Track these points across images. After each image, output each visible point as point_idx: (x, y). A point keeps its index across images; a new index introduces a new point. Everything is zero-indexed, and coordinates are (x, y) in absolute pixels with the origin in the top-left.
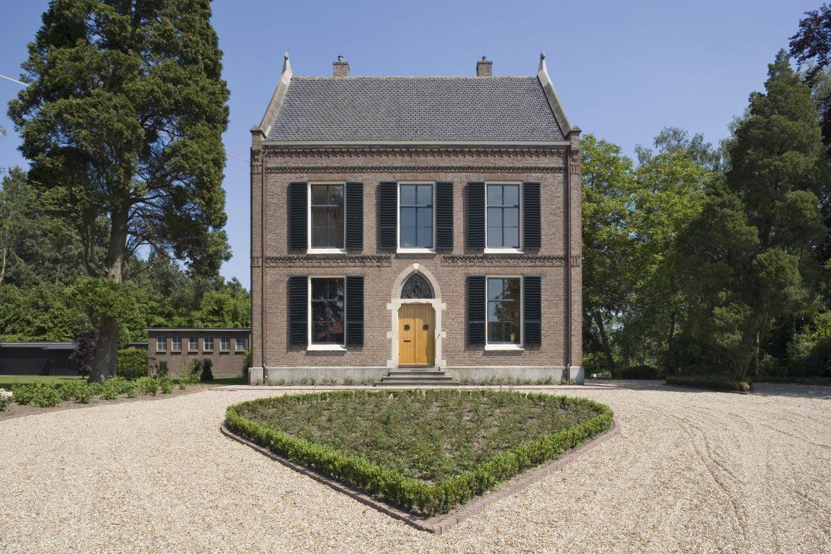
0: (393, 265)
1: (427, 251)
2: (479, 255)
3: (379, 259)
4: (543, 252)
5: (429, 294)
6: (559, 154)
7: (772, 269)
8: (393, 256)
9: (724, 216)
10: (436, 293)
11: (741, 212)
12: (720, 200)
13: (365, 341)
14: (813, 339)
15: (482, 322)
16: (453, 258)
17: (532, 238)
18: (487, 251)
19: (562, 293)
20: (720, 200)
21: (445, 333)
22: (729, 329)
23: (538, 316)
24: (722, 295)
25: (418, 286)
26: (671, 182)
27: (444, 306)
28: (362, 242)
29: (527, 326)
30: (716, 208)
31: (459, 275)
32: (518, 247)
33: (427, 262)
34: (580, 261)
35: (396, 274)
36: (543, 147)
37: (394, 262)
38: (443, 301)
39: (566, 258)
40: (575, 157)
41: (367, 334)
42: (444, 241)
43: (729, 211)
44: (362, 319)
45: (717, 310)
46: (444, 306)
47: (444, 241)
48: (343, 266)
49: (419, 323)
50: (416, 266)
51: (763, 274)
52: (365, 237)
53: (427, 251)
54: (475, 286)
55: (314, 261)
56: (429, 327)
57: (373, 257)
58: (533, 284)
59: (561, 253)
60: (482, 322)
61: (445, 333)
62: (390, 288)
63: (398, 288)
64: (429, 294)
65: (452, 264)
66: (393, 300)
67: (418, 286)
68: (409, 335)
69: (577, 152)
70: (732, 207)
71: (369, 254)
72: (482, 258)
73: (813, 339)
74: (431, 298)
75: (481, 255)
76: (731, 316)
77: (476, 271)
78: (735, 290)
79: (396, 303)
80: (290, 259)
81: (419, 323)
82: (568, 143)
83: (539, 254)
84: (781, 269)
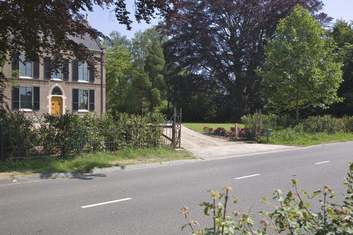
0: (49, 84)
1: (60, 80)
2: (76, 82)
3: (45, 81)
4: (95, 83)
5: (61, 93)
6: (100, 54)
7: (155, 93)
8: (49, 81)
9: (144, 79)
10: (63, 94)
11: (148, 78)
12: (143, 75)
13: (40, 108)
14: (159, 109)
15: (91, 103)
16: (69, 83)
17: (92, 79)
18: (79, 81)
19: (100, 95)
20: (143, 75)
21: (66, 106)
22: (146, 107)
23: (94, 102)
24: (144, 98)
25: (57, 91)
26: (277, 135)
27: (66, 98)
28: (39, 76)
29: (34, 103)
30: (143, 77)
31: (70, 88)
32: (87, 81)
33: (60, 83)
34: (105, 86)
35: (50, 87)
36: (95, 51)
37: (50, 83)
38: (65, 96)
39: (101, 85)
40: (104, 55)
41: (41, 106)
42: (66, 77)
43: (145, 78)
44: (39, 101)
45: (143, 102)
46: (66, 98)
47: (66, 77)
48: (20, 82)
49: (57, 103)
50: (57, 85)
51: (153, 94)
52: (40, 74)
53: (60, 80)
54: (75, 92)
55: (22, 81)
56: (61, 104)
57: (43, 81)
58: (92, 92)
59: (100, 83)
60: (91, 103)
61: (66, 106)
62: (48, 91)
63: (51, 91)
64: (61, 93)
65: (68, 85)
66: (49, 95)
67: (57, 91)
68: (54, 106)
69: (105, 54)
70: (146, 77)
71: (41, 80)
72: (77, 83)
73: (159, 109)
74: (61, 95)
75: (77, 82)
76: (146, 104)
77: (76, 87)
78: (146, 97)
79: (50, 96)
80: (13, 79)
81: (57, 103)
82: (102, 51)
83: (94, 83)
84: (157, 93)
